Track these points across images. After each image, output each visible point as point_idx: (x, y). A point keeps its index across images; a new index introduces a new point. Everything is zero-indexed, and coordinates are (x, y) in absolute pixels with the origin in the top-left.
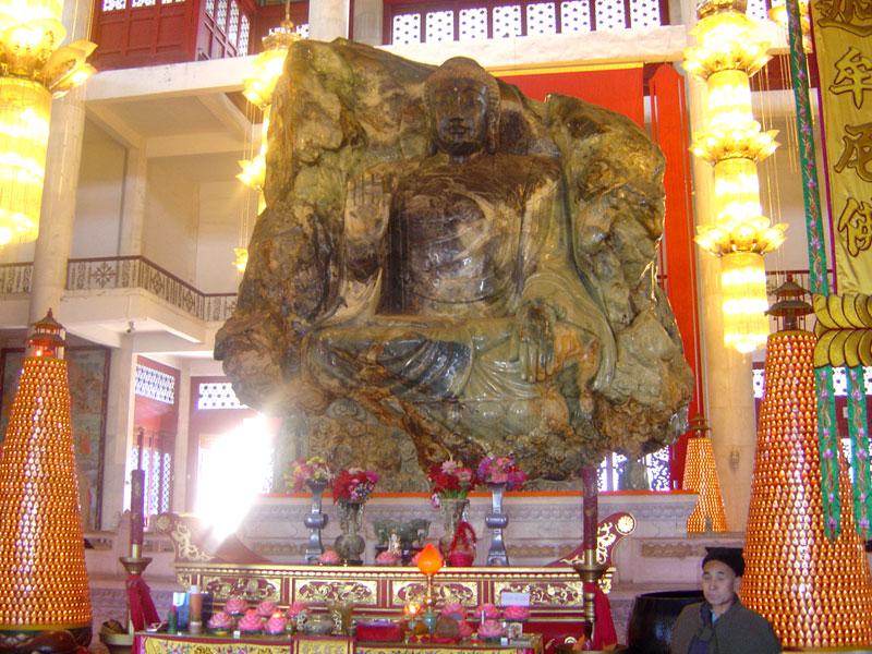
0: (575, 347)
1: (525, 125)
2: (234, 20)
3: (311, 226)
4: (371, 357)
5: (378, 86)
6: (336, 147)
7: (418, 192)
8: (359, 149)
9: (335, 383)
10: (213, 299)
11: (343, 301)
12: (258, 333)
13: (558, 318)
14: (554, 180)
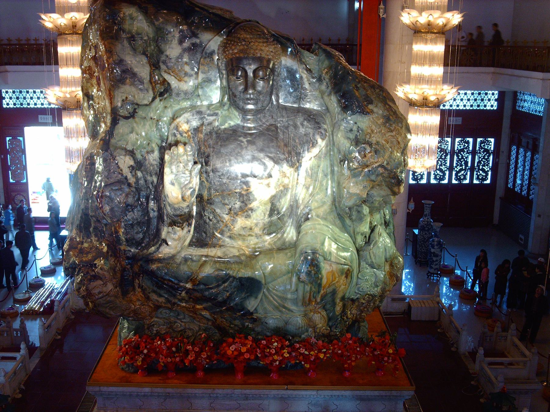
3: (133, 176)
4: (189, 286)
5: (177, 35)
11: (165, 242)
13: (325, 259)
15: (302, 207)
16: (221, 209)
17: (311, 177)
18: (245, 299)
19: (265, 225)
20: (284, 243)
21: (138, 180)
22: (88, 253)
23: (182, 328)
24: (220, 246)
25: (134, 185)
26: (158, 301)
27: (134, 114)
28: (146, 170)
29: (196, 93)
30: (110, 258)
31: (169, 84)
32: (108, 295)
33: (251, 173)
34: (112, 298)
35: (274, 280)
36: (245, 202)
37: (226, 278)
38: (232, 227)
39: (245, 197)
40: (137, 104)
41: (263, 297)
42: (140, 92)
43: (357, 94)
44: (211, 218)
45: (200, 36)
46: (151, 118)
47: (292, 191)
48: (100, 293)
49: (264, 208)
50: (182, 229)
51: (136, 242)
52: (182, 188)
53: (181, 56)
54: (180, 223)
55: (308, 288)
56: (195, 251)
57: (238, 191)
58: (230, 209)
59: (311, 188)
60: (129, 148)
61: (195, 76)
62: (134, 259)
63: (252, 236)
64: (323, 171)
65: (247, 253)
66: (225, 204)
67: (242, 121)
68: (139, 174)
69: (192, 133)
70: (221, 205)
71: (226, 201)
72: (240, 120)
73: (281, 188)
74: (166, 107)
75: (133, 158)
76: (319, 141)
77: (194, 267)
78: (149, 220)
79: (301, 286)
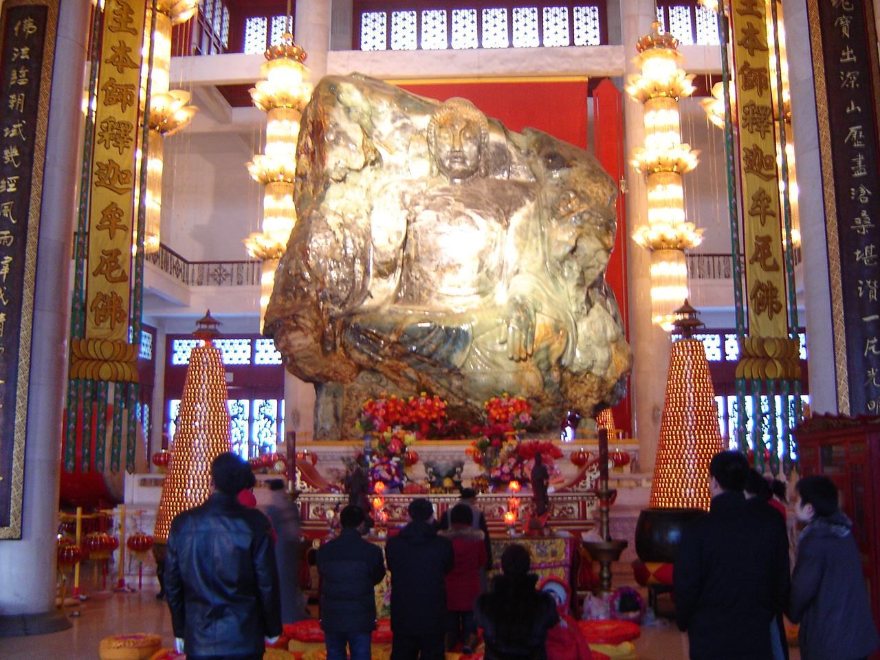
0: (548, 332)
1: (508, 154)
2: (218, 13)
7: (427, 208)
8: (376, 169)
9: (364, 358)
10: (196, 266)
11: (370, 294)
12: (304, 318)
14: (531, 201)
17: (521, 235)
26: (359, 360)
44: (418, 276)
53: (392, 134)
70: (428, 262)
77: (399, 318)
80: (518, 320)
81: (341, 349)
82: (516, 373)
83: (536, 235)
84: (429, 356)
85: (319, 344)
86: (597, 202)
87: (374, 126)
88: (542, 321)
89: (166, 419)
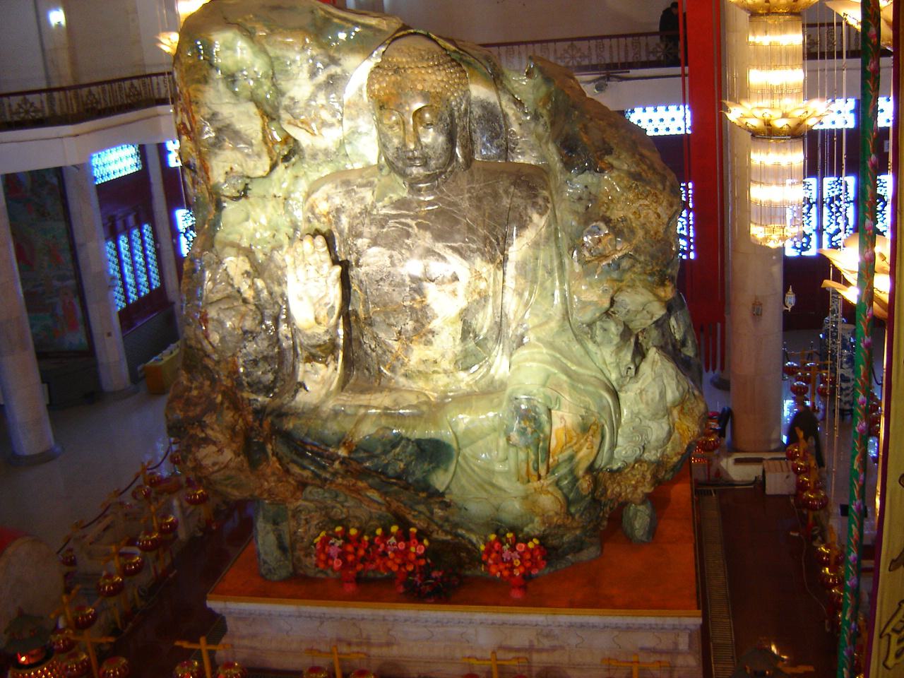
4: (342, 452)
5: (306, 66)
6: (265, 174)
7: (375, 242)
11: (302, 385)
14: (541, 214)
15: (514, 325)
16: (386, 332)
18: (429, 472)
19: (456, 355)
20: (492, 381)
21: (257, 293)
22: (196, 405)
23: (344, 516)
24: (391, 390)
25: (251, 300)
26: (302, 476)
27: (245, 193)
28: (271, 277)
29: (343, 152)
30: (226, 412)
31: (295, 140)
32: (226, 466)
33: (425, 273)
34: (233, 473)
35: (473, 442)
36: (421, 320)
37: (396, 441)
38: (406, 360)
39: (420, 313)
40: (248, 177)
41: (458, 469)
42: (248, 159)
43: (585, 140)
44: (373, 346)
45: (341, 62)
46: (275, 196)
47: (495, 301)
48: (214, 464)
49: (451, 329)
50: (327, 366)
51: (265, 387)
52: (314, 305)
53: (313, 97)
54: (322, 357)
55: (522, 455)
56: (350, 399)
57: (407, 303)
58: (400, 333)
59: (526, 294)
60: (245, 243)
61: (337, 125)
62: (260, 413)
63: (439, 373)
64: (544, 266)
65: (433, 399)
66: (390, 325)
67: (409, 192)
68: (260, 283)
69: (334, 217)
70: (385, 327)
71: (392, 321)
72: (407, 191)
73: (476, 297)
74: (296, 177)
75: (249, 260)
76: (535, 217)
77: (348, 425)
78: (282, 353)
79: (512, 451)
80: (522, 432)
81: (274, 459)
82: (525, 498)
83: (550, 273)
84: (398, 477)
85: (242, 457)
86: (647, 232)
87: (280, 93)
88: (563, 419)
89: (175, 233)
